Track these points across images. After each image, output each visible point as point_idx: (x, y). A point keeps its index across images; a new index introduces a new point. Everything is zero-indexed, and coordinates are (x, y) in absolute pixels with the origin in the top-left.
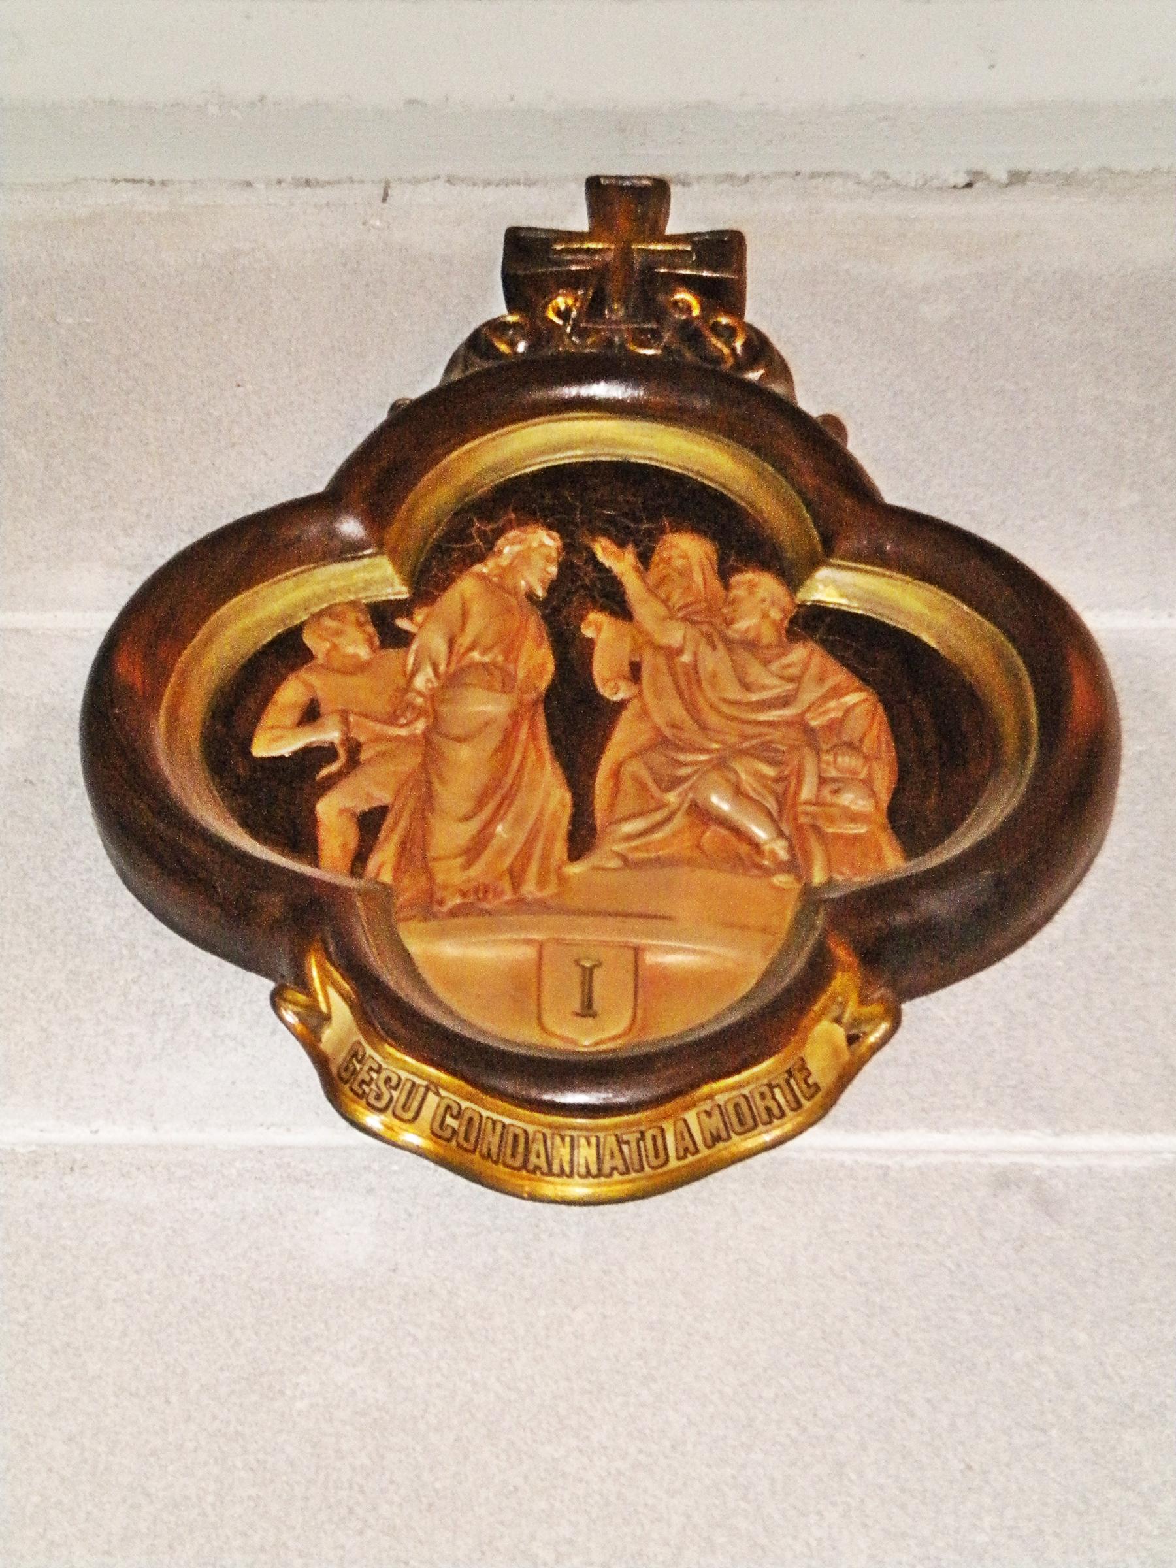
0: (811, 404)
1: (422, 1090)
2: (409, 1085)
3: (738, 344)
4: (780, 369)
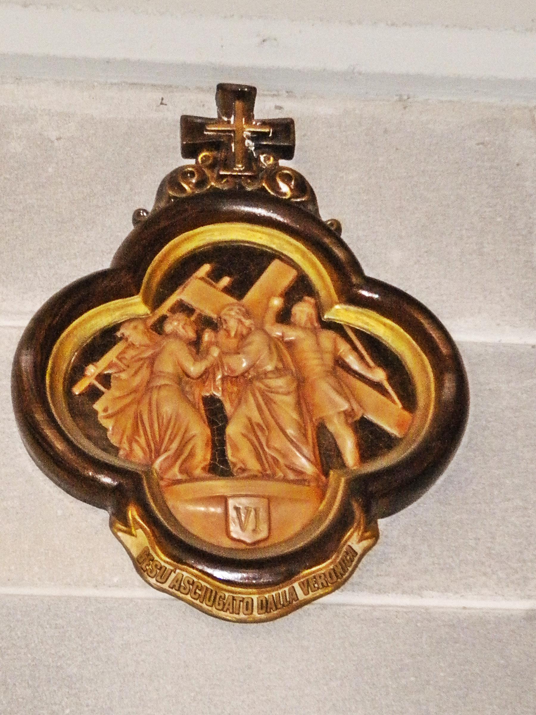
0: (325, 216)
2: (164, 569)
4: (313, 199)
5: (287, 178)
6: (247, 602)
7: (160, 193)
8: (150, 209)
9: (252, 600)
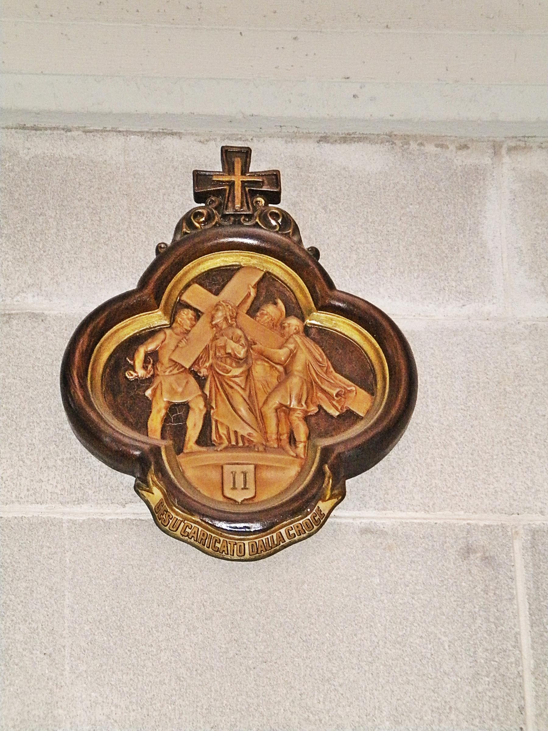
1: (179, 522)
3: (280, 221)
5: (275, 216)
6: (240, 546)
7: (178, 228)
8: (169, 242)
9: (244, 544)
